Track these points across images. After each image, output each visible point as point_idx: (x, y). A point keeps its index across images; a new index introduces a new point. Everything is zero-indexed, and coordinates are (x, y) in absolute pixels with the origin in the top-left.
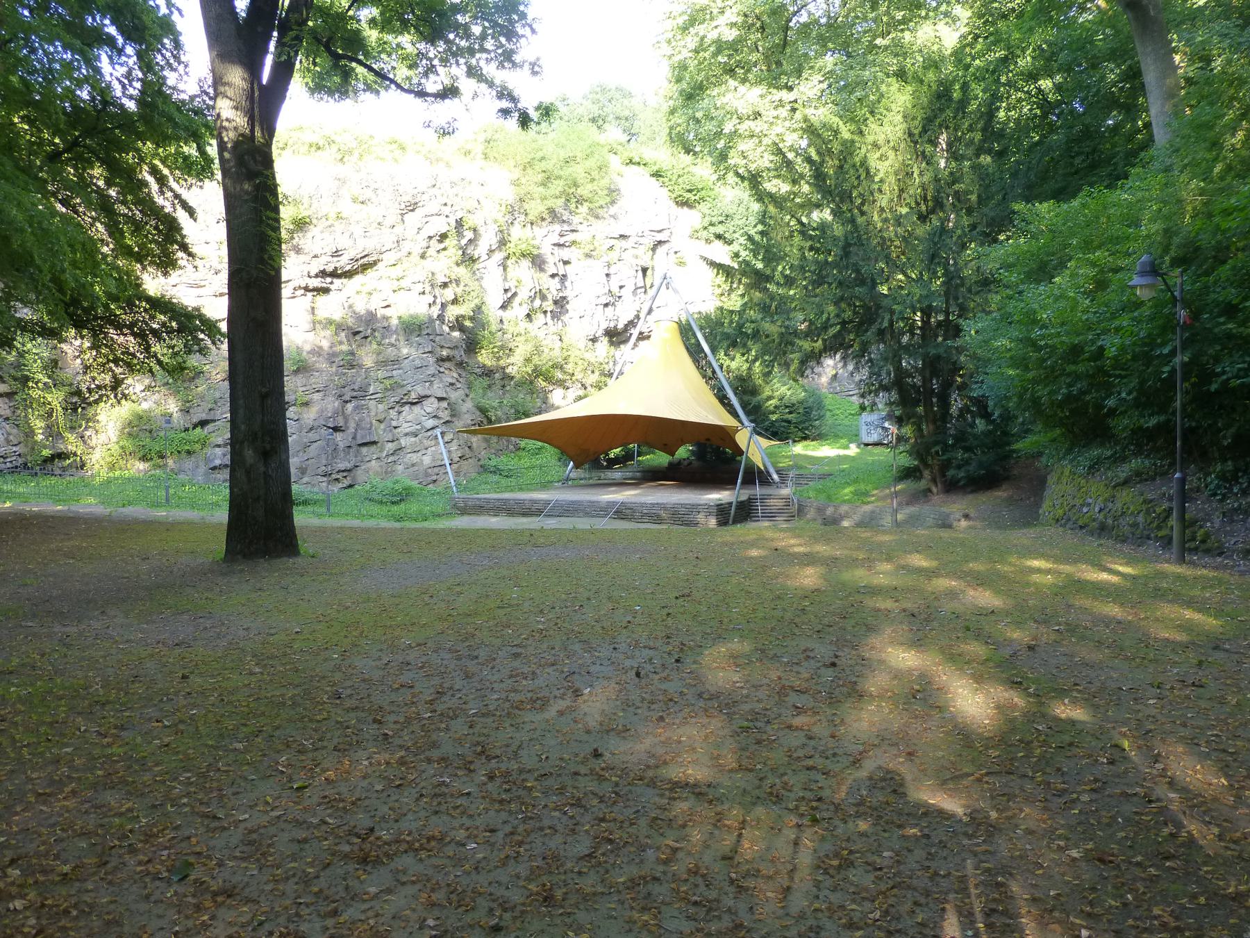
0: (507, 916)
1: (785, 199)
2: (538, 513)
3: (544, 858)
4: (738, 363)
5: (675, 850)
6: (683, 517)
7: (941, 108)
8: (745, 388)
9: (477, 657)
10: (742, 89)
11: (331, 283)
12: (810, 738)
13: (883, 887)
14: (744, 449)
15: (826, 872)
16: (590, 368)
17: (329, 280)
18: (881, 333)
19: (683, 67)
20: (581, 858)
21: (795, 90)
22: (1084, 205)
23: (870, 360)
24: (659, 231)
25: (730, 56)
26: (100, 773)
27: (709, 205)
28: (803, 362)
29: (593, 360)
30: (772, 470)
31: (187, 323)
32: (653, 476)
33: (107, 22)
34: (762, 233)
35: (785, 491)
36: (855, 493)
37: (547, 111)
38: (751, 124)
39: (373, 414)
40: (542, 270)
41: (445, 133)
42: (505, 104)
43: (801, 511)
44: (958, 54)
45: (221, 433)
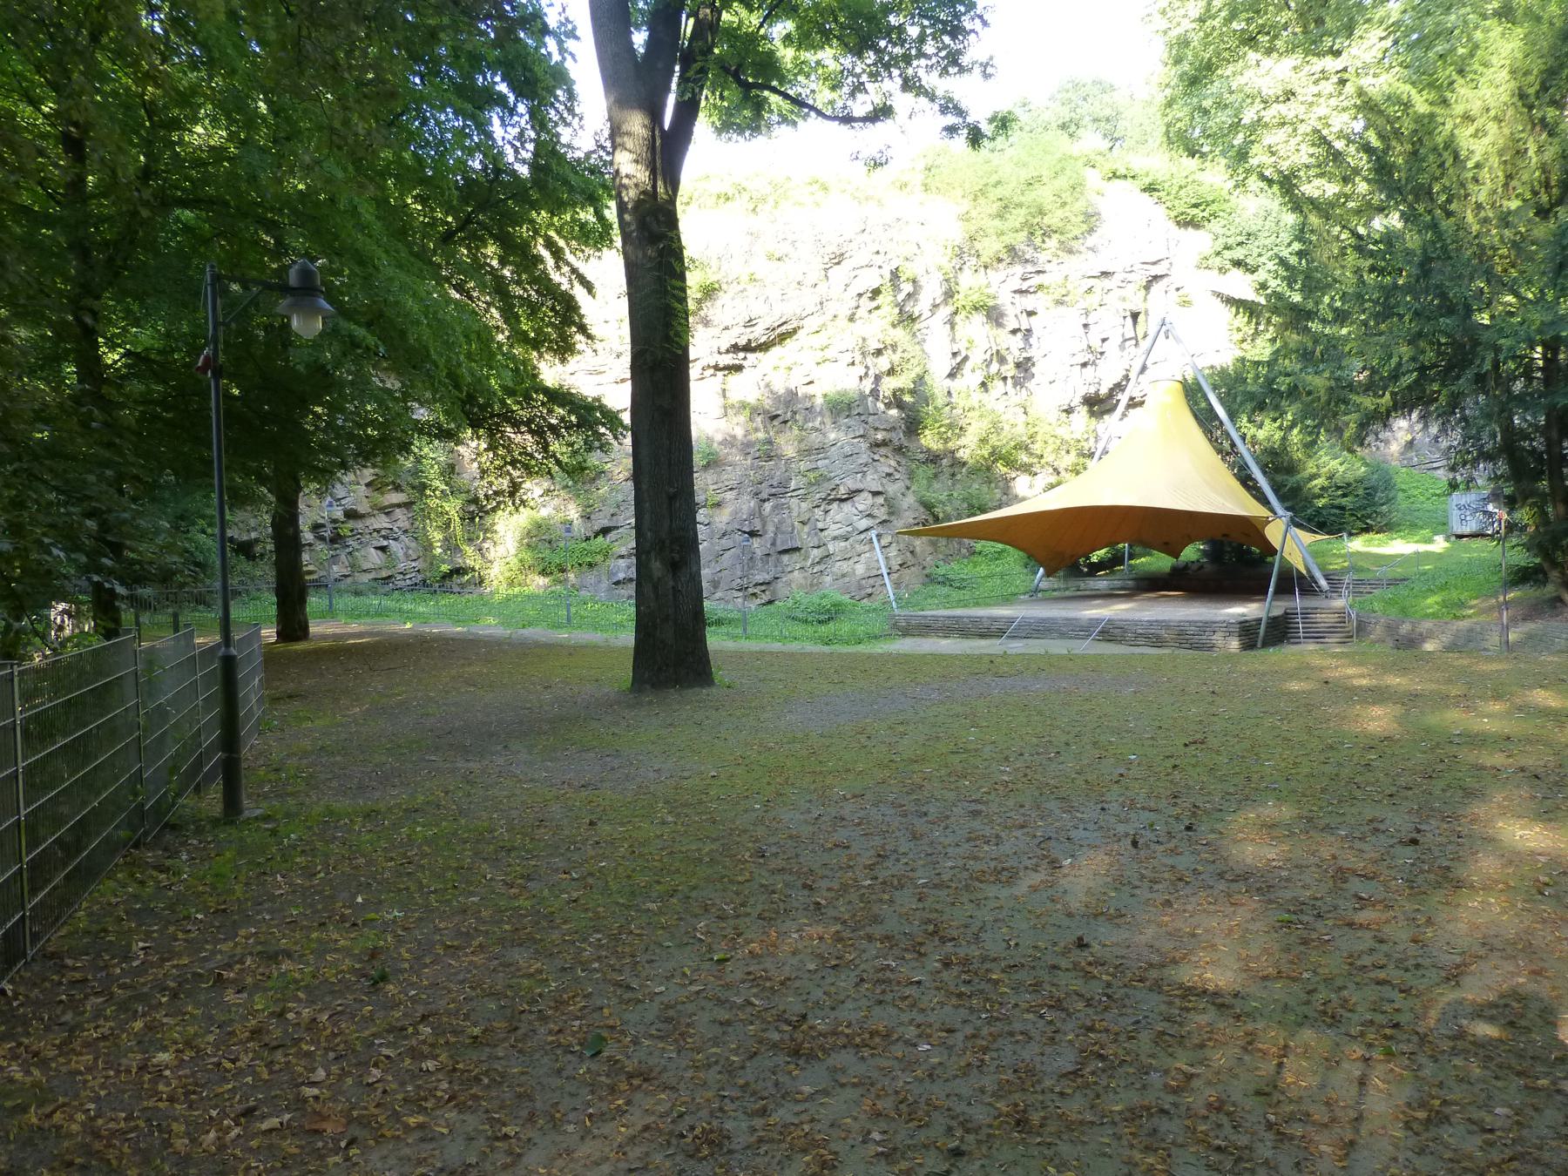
0: (971, 1138)
1: (1332, 204)
2: (999, 633)
4: (1267, 431)
5: (1190, 1077)
6: (1191, 639)
8: (1278, 464)
10: (1267, 62)
12: (1381, 941)
13: (1496, 1156)
16: (1064, 447)
17: (741, 355)
18: (1480, 379)
19: (1184, 43)
20: (1064, 1075)
24: (1154, 263)
26: (507, 927)
27: (1223, 222)
28: (1363, 426)
29: (1067, 437)
30: (1318, 575)
32: (1151, 585)
33: (498, 79)
34: (1300, 254)
35: (1339, 603)
36: (1444, 604)
37: (1003, 123)
38: (1282, 108)
39: (795, 514)
40: (999, 325)
42: (951, 119)
43: (1362, 628)
45: (625, 542)
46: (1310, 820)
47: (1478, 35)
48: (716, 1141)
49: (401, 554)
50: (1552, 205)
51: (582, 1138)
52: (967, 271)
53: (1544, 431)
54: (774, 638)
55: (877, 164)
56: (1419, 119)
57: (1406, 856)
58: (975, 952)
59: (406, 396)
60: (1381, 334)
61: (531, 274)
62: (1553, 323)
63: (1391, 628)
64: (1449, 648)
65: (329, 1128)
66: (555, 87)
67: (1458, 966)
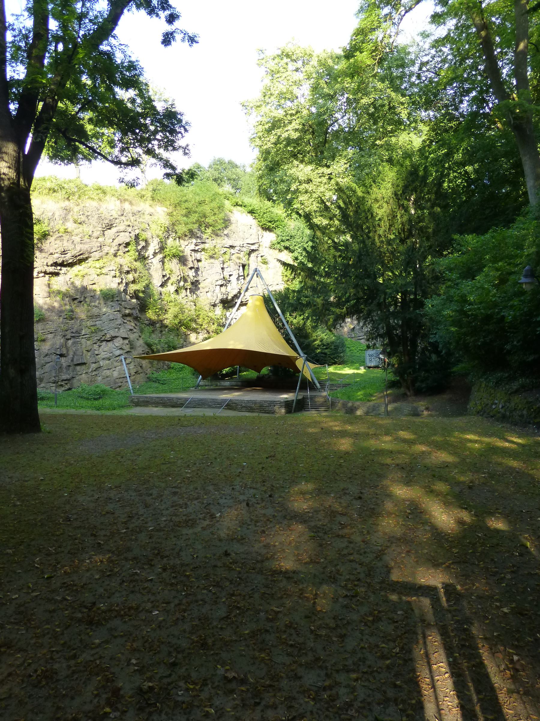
0: (180, 656)
1: (325, 228)
3: (199, 620)
5: (277, 613)
6: (264, 408)
7: (413, 181)
9: (151, 495)
10: (301, 166)
11: (61, 270)
12: (351, 543)
13: (399, 633)
15: (366, 625)
16: (212, 321)
17: (59, 268)
18: (379, 305)
19: (268, 152)
22: (493, 237)
23: (372, 320)
25: (295, 147)
27: (281, 230)
28: (336, 320)
29: (213, 317)
30: (316, 382)
32: (247, 385)
35: (325, 394)
36: (365, 395)
37: (192, 175)
39: (84, 346)
41: (132, 186)
42: (169, 171)
43: (333, 404)
44: (421, 151)
46: (319, 490)
47: (380, 168)
50: (406, 239)
53: (401, 327)
55: (132, 186)
56: (358, 198)
57: (357, 504)
60: (343, 283)
62: (405, 285)
63: (344, 405)
64: (367, 413)
67: (380, 551)
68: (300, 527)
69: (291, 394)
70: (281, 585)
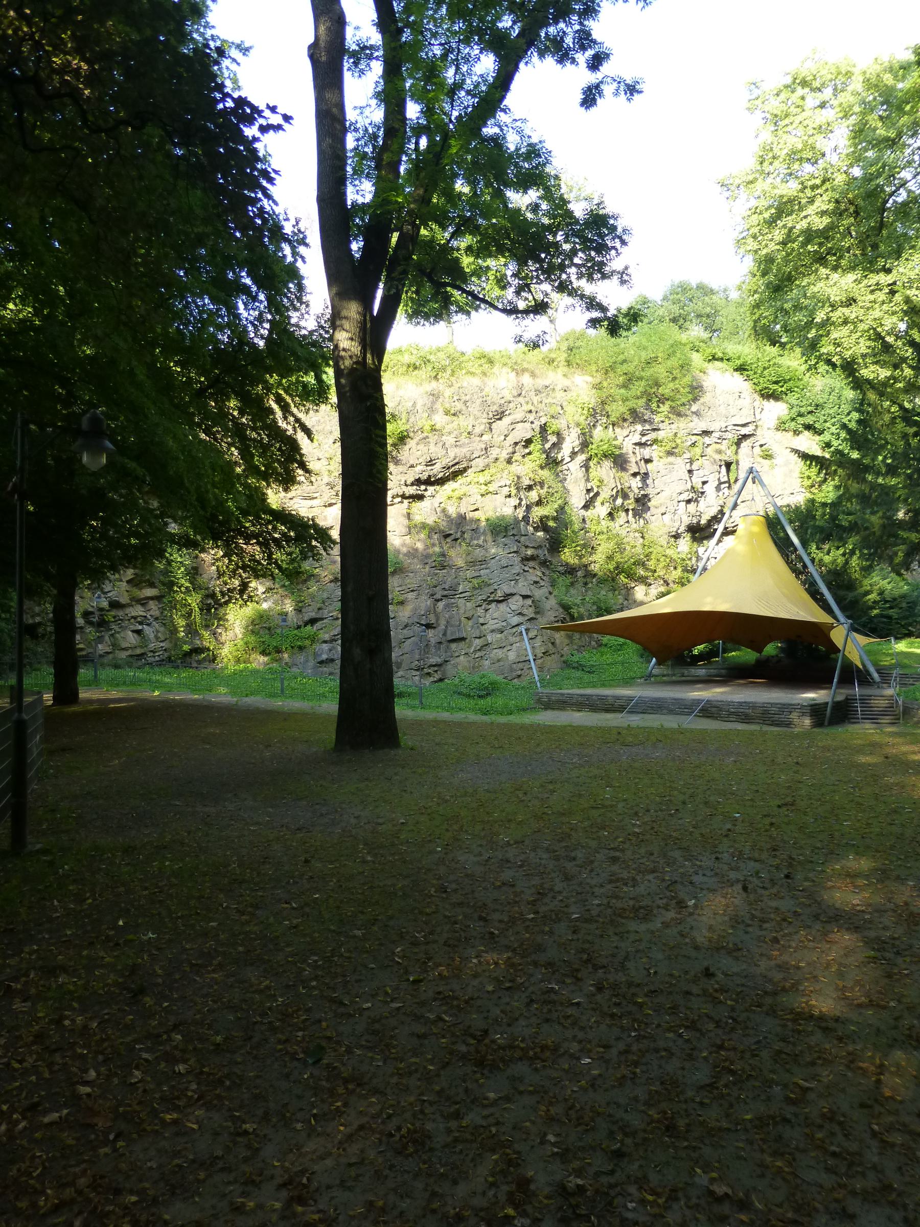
0: (629, 1141)
1: (885, 384)
2: (620, 709)
3: (662, 1083)
8: (840, 581)
9: (574, 859)
10: (835, 276)
14: (840, 647)
16: (672, 564)
17: (423, 487)
19: (769, 260)
20: (702, 1088)
21: (894, 271)
24: (744, 425)
25: (821, 245)
26: (241, 949)
27: (797, 396)
29: (675, 556)
30: (872, 670)
31: (304, 532)
32: (738, 674)
33: (243, 274)
35: (889, 692)
37: (634, 316)
38: (846, 310)
39: (462, 611)
42: (596, 314)
45: (331, 628)
46: (884, 872)
48: (419, 1140)
49: (152, 636)
51: (309, 1135)
52: (599, 428)
54: (443, 709)
55: (536, 346)
58: (621, 977)
59: (162, 516)
61: (264, 422)
65: (101, 1123)
66: (288, 282)
68: (847, 938)
69: (823, 692)
70: (813, 1040)
